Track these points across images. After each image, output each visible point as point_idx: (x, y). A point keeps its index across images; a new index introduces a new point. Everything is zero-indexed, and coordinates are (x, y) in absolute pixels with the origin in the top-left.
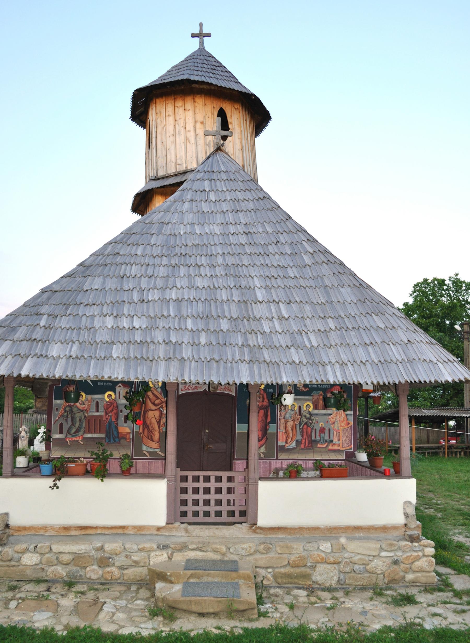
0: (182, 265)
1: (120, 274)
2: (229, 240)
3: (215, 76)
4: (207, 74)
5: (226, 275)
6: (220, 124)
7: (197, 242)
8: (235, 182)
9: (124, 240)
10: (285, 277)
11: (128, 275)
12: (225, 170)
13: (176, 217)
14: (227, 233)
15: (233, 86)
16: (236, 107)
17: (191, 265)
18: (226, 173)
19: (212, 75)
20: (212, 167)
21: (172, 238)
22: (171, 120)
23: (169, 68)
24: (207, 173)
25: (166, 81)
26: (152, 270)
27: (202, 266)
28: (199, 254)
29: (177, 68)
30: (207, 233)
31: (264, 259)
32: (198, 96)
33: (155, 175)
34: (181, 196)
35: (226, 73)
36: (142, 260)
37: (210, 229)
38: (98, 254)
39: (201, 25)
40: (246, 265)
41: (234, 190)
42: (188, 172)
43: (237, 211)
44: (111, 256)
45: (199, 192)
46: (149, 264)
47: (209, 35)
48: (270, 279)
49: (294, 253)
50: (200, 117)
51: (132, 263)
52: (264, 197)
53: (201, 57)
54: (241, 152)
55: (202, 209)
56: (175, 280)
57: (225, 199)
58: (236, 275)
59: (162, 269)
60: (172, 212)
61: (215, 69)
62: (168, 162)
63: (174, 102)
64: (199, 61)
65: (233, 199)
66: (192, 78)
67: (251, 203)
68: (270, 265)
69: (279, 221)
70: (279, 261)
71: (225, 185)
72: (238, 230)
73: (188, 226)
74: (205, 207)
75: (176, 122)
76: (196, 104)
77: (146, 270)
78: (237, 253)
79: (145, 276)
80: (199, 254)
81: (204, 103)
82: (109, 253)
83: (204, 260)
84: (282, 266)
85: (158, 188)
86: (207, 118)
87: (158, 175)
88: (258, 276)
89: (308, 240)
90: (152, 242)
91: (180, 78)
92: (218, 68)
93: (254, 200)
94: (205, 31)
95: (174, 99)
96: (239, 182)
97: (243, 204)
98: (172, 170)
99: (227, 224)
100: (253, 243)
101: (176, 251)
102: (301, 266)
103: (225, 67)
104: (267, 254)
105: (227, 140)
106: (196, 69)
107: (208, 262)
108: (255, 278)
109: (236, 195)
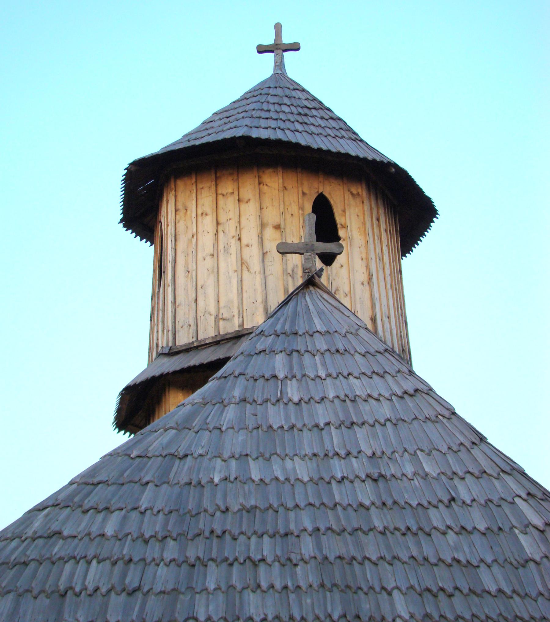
0: (212, 560)
1: (57, 586)
2: (332, 496)
3: (306, 128)
4: (288, 125)
5: (322, 585)
6: (314, 229)
7: (253, 502)
8: (347, 355)
9: (76, 499)
10: (475, 593)
11: (77, 589)
12: (323, 329)
13: (204, 441)
14: (327, 479)
15: (346, 147)
16: (355, 192)
17: (236, 559)
18: (328, 337)
19: (299, 127)
20: (293, 322)
21: (193, 492)
22: (208, 223)
23: (207, 115)
24: (282, 337)
25: (197, 143)
26: (138, 574)
27: (262, 564)
28: (255, 533)
29: (225, 115)
30: (277, 479)
31: (419, 545)
32: (269, 171)
33: (170, 345)
34: (220, 390)
35: (330, 121)
36: (115, 549)
37: (284, 469)
38: (9, 535)
39: (278, 28)
40: (374, 558)
41: (345, 374)
42: (244, 335)
43: (353, 423)
44: (41, 541)
45: (261, 382)
46: (131, 560)
47: (295, 47)
48: (435, 596)
49: (496, 529)
50: (272, 215)
51: (89, 557)
52: (416, 390)
53: (279, 91)
54: (367, 287)
55: (267, 419)
56: (192, 602)
57: (321, 395)
58: (348, 587)
59: (162, 570)
60: (196, 429)
61: (306, 115)
62: (200, 314)
63: (216, 185)
64: (271, 99)
65: (342, 396)
66: (255, 134)
67: (386, 405)
68: (433, 560)
69: (455, 448)
70: (456, 548)
71: (324, 364)
72: (353, 470)
73: (233, 463)
74: (276, 416)
75: (220, 229)
76: (265, 188)
77: (124, 575)
78: (349, 529)
79: (119, 589)
80: (255, 533)
81: (281, 186)
82: (35, 532)
83: (268, 548)
84: (464, 561)
85: (175, 373)
86: (288, 216)
87: (177, 344)
88: (404, 589)
89: (529, 494)
90: (144, 504)
91: (228, 135)
92: (314, 112)
93: (394, 398)
94: (287, 39)
95: (217, 179)
96: (357, 356)
97: (365, 407)
98: (208, 332)
99: (326, 455)
100: (389, 502)
101: (201, 526)
102: (515, 563)
103: (329, 110)
104: (427, 529)
105: (335, 264)
106: (264, 115)
107: (279, 553)
108: (395, 593)
109: (350, 387)
